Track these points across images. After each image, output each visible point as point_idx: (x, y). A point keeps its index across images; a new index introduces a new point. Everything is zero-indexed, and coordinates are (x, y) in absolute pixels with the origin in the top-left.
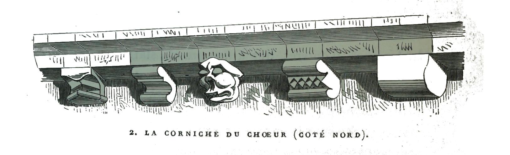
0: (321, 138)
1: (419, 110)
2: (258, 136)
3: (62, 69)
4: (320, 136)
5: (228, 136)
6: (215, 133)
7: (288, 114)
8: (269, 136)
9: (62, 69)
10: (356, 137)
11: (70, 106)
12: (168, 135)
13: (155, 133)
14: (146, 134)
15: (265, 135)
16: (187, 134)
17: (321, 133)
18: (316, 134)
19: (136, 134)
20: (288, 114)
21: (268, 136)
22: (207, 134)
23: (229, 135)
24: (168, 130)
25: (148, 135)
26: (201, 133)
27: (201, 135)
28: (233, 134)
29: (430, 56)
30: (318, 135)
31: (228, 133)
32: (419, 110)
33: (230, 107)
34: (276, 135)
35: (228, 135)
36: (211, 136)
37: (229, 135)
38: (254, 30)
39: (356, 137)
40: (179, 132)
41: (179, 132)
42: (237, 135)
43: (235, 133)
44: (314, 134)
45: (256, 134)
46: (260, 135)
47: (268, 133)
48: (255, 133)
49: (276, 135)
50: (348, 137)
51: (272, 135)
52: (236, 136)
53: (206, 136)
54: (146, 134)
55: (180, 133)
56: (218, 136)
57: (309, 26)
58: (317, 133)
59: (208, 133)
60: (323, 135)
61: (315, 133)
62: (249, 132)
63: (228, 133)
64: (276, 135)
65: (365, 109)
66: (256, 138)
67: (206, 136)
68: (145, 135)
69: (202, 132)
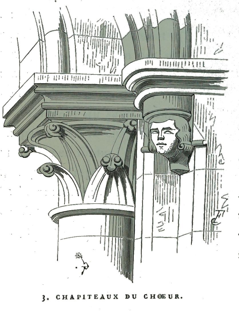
1: (95, 26)
2: (154, 298)
4: (94, 298)
5: (126, 298)
6: (95, 295)
7: (162, 231)
8: (164, 297)
10: (126, 298)
11: (17, 134)
12: (59, 299)
13: (73, 298)
15: (160, 296)
18: (90, 296)
20: (162, 231)
21: (163, 298)
22: (151, 297)
23: (127, 297)
26: (58, 296)
27: (146, 297)
28: (131, 296)
30: (92, 297)
31: (126, 295)
32: (95, 26)
33: (105, 55)
34: (170, 297)
36: (155, 298)
37: (127, 297)
40: (176, 295)
41: (176, 295)
42: (171, 297)
43: (133, 295)
44: (89, 296)
45: (65, 296)
46: (156, 296)
47: (163, 295)
48: (63, 296)
49: (109, 297)
50: (176, 298)
51: (167, 296)
52: (108, 298)
53: (151, 298)
55: (72, 298)
58: (91, 295)
59: (65, 296)
61: (90, 295)
62: (145, 295)
63: (126, 295)
64: (170, 297)
65: (94, 27)
66: (153, 299)
67: (151, 298)
68: (126, 298)
69: (59, 296)
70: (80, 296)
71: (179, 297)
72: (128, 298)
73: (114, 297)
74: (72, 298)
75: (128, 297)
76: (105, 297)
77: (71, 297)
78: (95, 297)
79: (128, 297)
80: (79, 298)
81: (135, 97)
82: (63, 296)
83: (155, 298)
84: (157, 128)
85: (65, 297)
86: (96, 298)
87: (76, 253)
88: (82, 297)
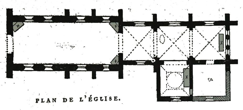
0: (115, 101)
2: (106, 100)
3: (165, 62)
5: (64, 101)
9: (165, 62)
10: (64, 101)
13: (49, 101)
14: (81, 101)
16: (53, 101)
17: (89, 98)
19: (119, 100)
23: (65, 100)
24: (97, 97)
25: (83, 101)
29: (13, 25)
31: (64, 99)
34: (13, 44)
35: (64, 100)
36: (107, 101)
37: (65, 100)
38: (196, 57)
39: (63, 102)
44: (43, 101)
54: (81, 101)
55: (49, 101)
56: (73, 101)
57: (183, 53)
60: (72, 100)
63: (64, 99)
70: (39, 100)
71: (118, 98)
72: (65, 102)
73: (19, 27)
74: (48, 102)
75: (65, 100)
76: (51, 100)
77: (48, 101)
78: (13, 42)
79: (65, 100)
80: (38, 102)
81: (196, 100)
82: (63, 100)
83: (107, 101)
84: (230, 100)
85: (7, 46)
86: (90, 100)
87: (55, 101)
88: (40, 100)
